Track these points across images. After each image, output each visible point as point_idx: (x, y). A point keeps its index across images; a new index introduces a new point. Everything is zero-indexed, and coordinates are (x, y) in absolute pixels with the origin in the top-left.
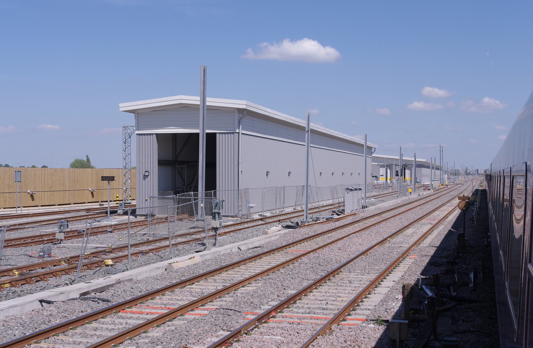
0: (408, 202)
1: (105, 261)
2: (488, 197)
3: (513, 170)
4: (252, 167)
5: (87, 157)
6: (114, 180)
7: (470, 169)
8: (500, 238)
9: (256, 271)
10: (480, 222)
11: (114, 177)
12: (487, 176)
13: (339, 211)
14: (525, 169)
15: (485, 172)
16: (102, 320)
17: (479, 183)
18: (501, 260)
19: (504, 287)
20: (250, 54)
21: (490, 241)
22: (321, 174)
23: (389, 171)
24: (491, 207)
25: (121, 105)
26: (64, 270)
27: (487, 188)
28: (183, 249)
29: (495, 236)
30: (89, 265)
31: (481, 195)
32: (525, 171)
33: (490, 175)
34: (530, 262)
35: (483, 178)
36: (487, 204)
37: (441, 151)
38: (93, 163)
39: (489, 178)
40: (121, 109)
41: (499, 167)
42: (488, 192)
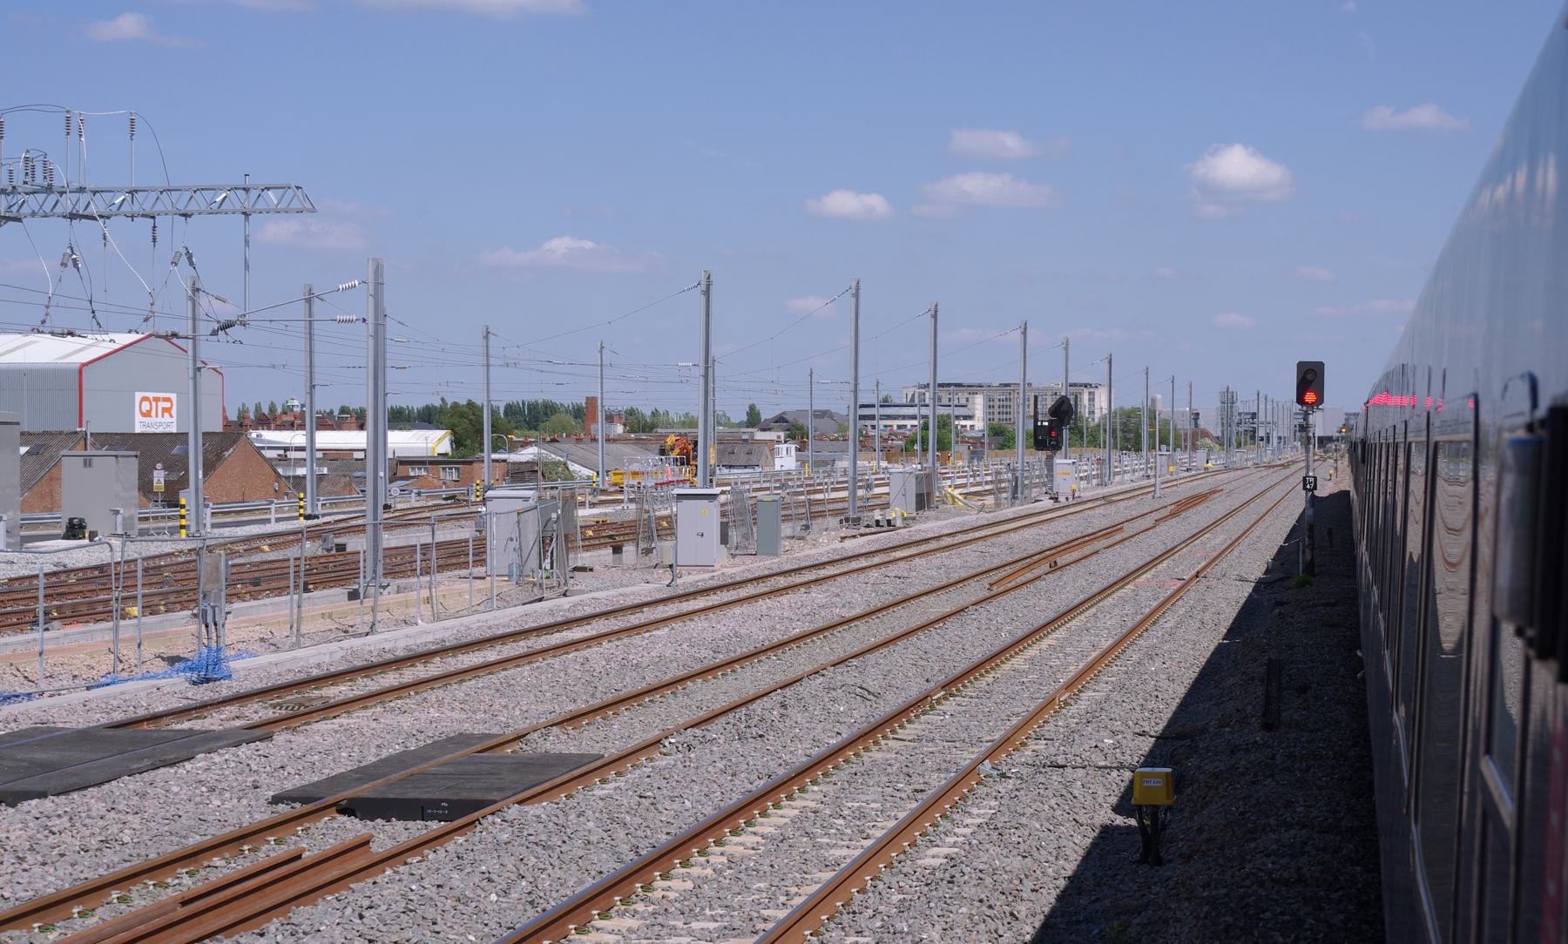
3: (1436, 421)
5: (752, 408)
8: (1396, 667)
12: (1353, 447)
13: (1063, 411)
14: (1472, 418)
18: (1398, 745)
21: (1363, 680)
24: (1366, 558)
29: (1381, 659)
32: (1471, 427)
33: (1364, 442)
34: (1488, 751)
36: (1352, 546)
38: (1470, 390)
41: (1383, 424)
42: (1353, 494)
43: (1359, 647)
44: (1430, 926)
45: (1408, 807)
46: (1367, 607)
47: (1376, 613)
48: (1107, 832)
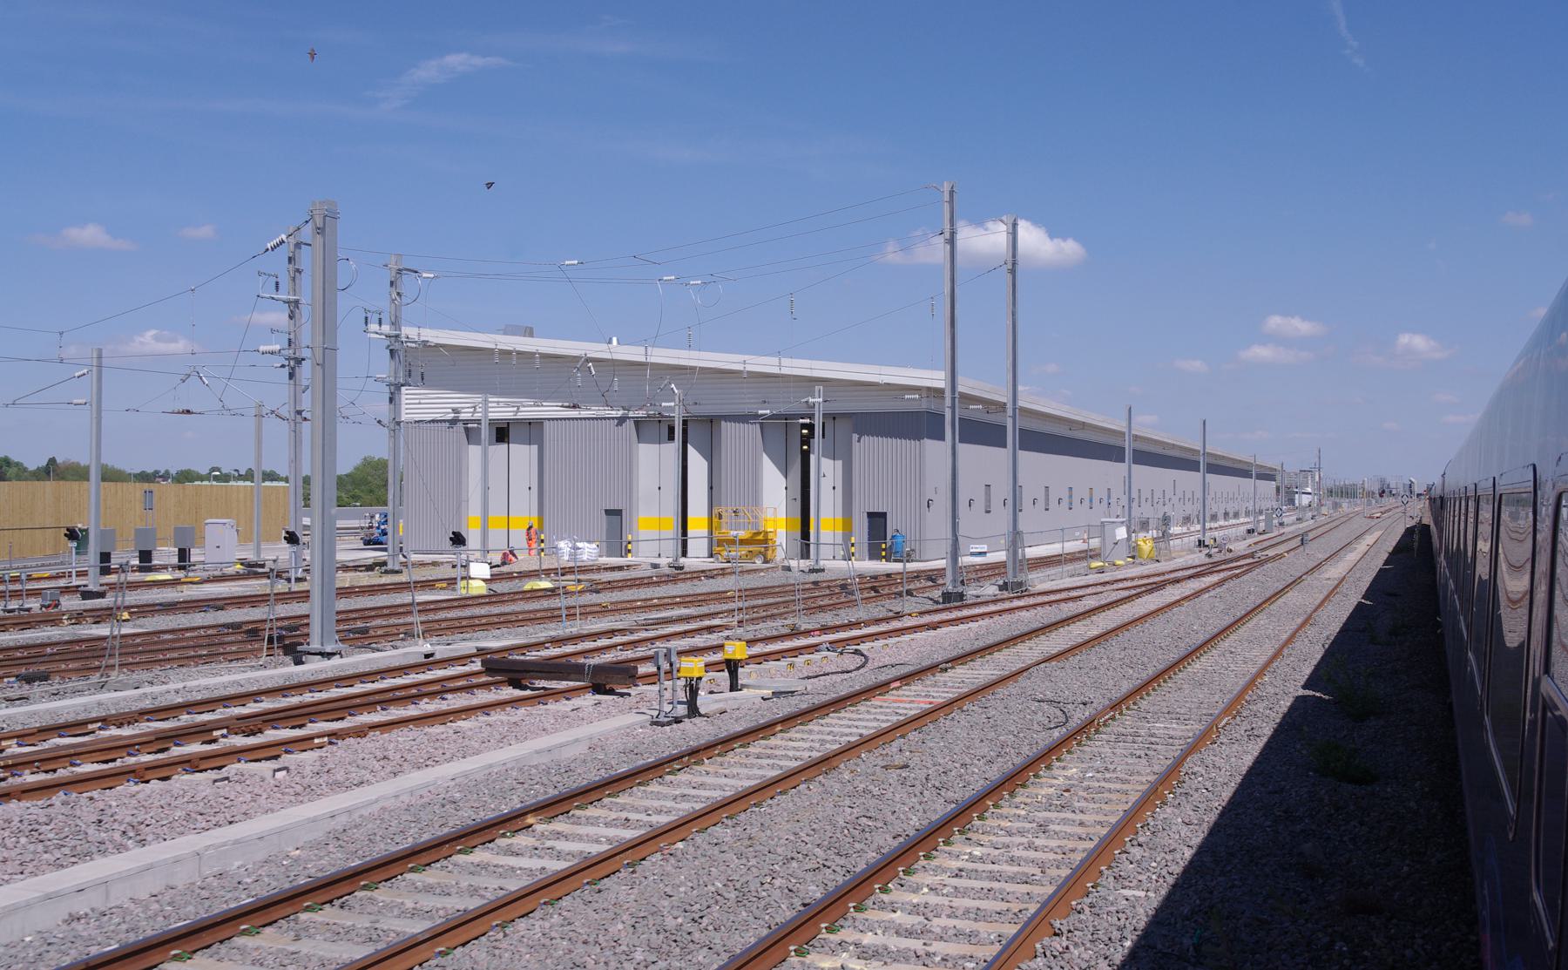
0: (980, 644)
6: (884, 515)
9: (655, 819)
10: (1419, 613)
11: (870, 515)
12: (1432, 500)
15: (1429, 489)
16: (578, 812)
17: (1419, 511)
19: (1482, 727)
20: (892, 255)
23: (698, 464)
24: (1444, 563)
28: (323, 770)
33: (1442, 498)
39: (1439, 504)
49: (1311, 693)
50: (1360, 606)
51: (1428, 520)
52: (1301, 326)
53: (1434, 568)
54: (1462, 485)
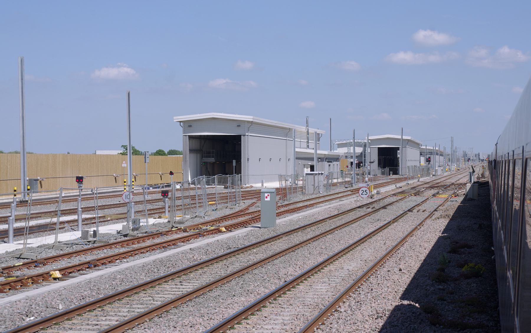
1: (51, 273)
2: (492, 193)
4: (409, 159)
7: (471, 155)
10: (480, 212)
12: (490, 162)
13: (469, 159)
17: (481, 171)
21: (494, 260)
22: (171, 173)
24: (496, 208)
25: (175, 118)
26: (42, 275)
27: (490, 181)
29: (502, 250)
30: (45, 275)
31: (481, 187)
33: (495, 161)
35: (486, 164)
37: (452, 141)
39: (494, 165)
40: (175, 121)
41: (503, 151)
43: (493, 246)
44: (517, 326)
45: (514, 310)
46: (496, 229)
47: (500, 231)
48: (397, 308)
49: (406, 302)
50: (440, 238)
51: (488, 178)
52: (439, 38)
53: (490, 211)
54: (506, 152)
